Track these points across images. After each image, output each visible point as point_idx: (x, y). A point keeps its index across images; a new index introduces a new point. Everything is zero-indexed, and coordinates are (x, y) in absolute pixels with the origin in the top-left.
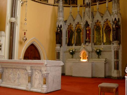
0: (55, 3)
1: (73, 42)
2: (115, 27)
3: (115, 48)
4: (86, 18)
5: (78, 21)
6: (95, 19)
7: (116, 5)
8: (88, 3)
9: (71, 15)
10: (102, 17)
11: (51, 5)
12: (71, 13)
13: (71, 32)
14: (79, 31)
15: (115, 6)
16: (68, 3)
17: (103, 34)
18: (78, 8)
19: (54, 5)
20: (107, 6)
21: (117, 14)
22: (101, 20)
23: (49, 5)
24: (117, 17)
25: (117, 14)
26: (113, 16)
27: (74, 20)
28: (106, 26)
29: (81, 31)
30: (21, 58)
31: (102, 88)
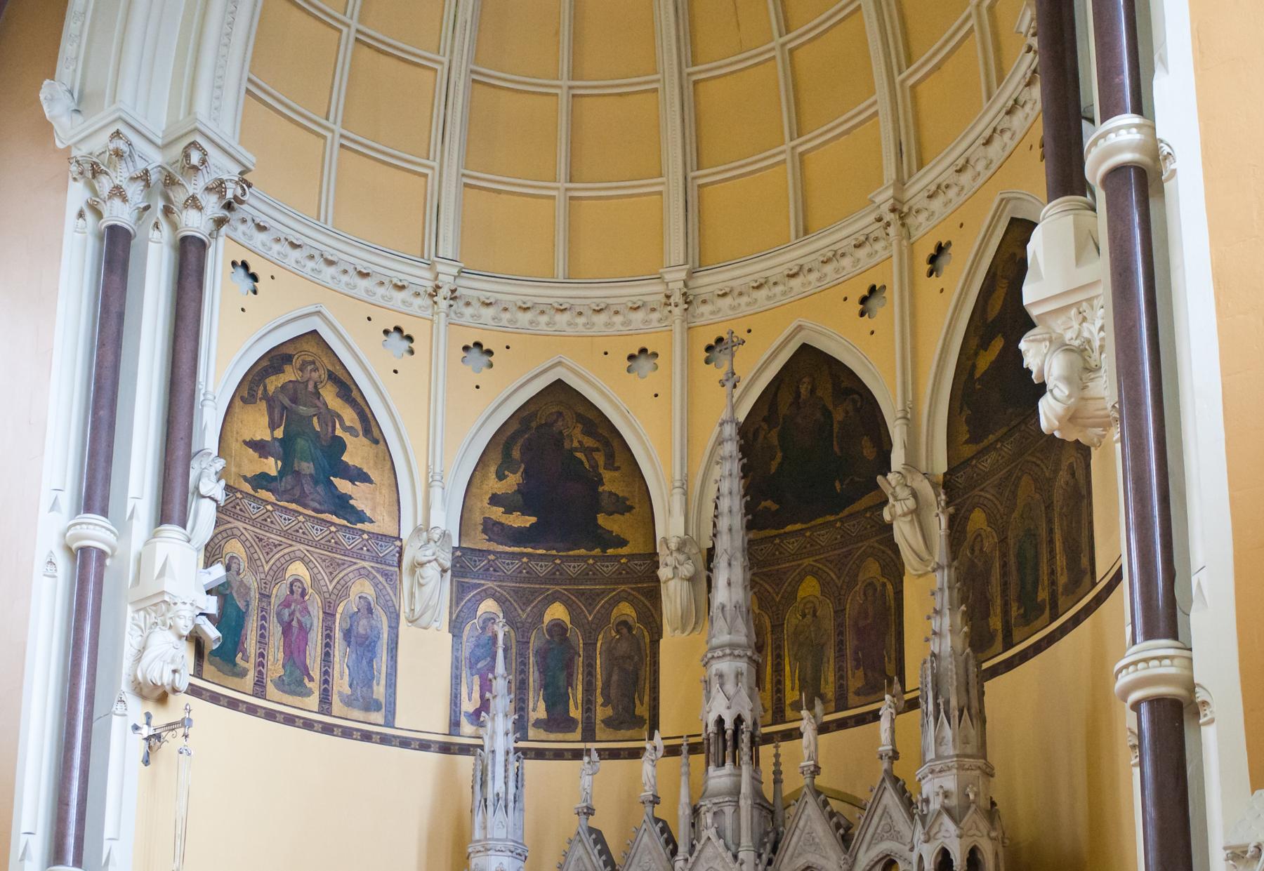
0: (455, 725)
4: (709, 851)
7: (948, 733)
8: (729, 725)
9: (585, 836)
11: (424, 746)
12: (589, 811)
15: (939, 741)
16: (573, 721)
19: (446, 749)
20: (886, 747)
23: (405, 743)
24: (960, 837)
25: (956, 812)
26: (922, 837)
30: (1024, 29)
31: (335, 422)
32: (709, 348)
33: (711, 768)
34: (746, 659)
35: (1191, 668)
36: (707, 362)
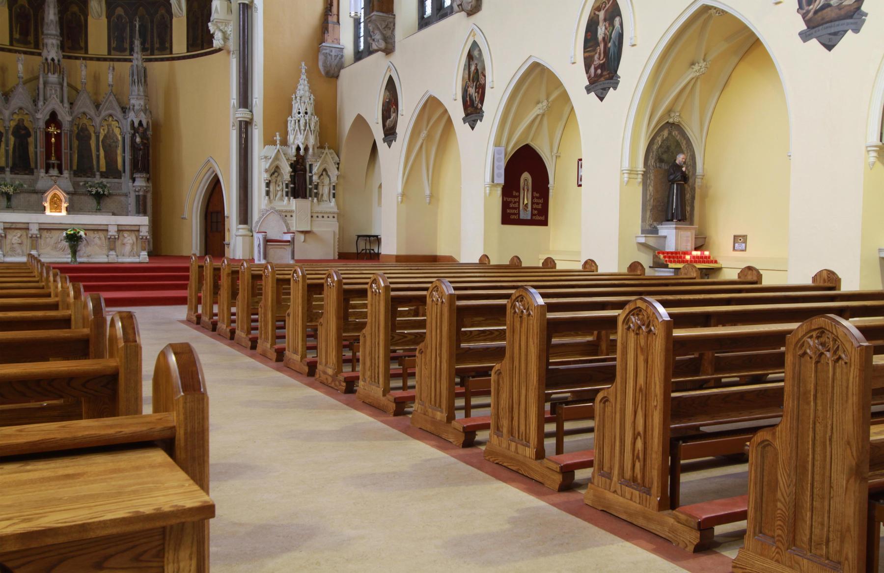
2: (142, 141)
3: (142, 189)
4: (53, 101)
5: (20, 104)
6: (76, 108)
7: (141, 89)
14: (23, 132)
15: (139, 90)
17: (98, 150)
21: (324, 173)
22: (94, 116)
23: (179, 58)
29: (28, 135)
35: (252, 115)
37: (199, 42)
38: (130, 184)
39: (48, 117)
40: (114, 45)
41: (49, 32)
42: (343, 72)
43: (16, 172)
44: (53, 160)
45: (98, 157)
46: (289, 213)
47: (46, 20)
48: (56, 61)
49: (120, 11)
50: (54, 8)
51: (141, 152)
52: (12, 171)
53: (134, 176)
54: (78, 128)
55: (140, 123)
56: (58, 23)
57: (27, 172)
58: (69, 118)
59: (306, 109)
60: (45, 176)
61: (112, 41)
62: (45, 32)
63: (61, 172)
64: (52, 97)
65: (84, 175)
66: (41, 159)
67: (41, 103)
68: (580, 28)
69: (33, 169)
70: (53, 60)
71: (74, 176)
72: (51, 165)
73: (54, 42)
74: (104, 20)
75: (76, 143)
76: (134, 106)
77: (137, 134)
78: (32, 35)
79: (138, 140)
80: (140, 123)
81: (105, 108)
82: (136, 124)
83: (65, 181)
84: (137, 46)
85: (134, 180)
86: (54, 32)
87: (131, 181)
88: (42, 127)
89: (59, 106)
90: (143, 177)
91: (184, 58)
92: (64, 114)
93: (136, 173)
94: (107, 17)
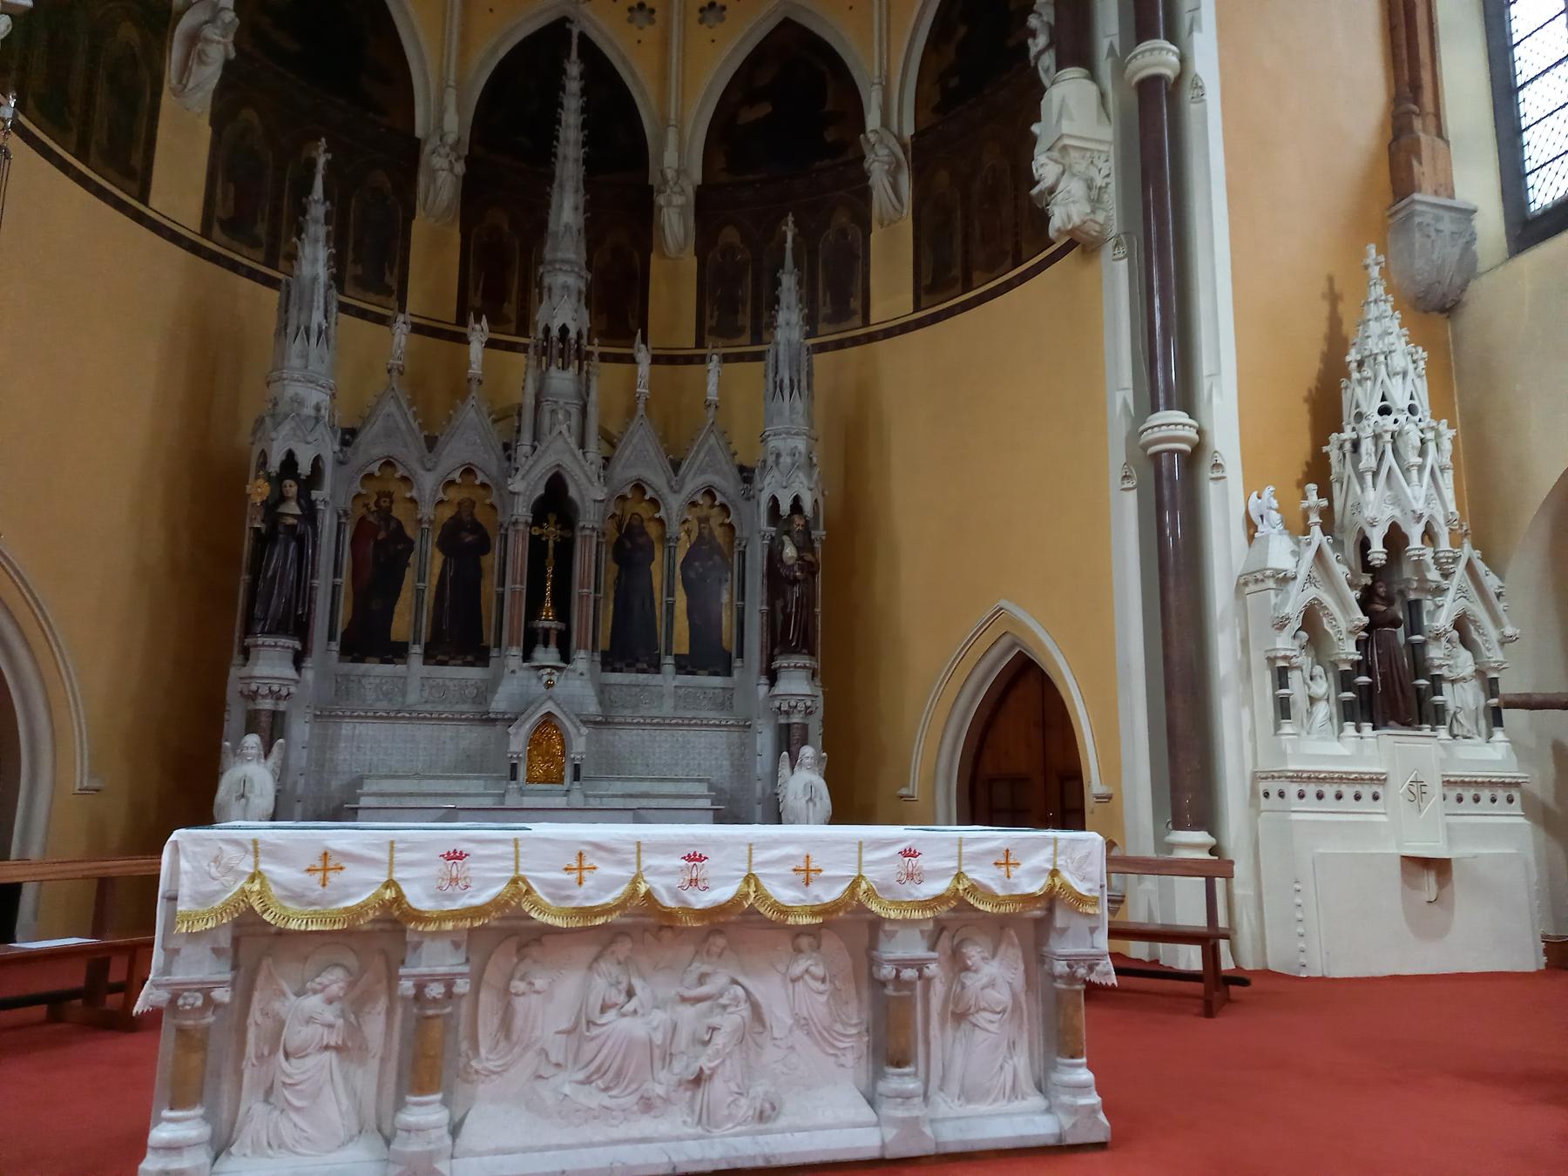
1: (400, 627)
2: (800, 558)
4: (559, 444)
6: (618, 469)
10: (676, 466)
13: (381, 536)
15: (792, 409)
17: (671, 593)
18: (400, 334)
19: (194, 248)
22: (665, 490)
23: (888, 333)
27: (431, 443)
28: (694, 536)
29: (484, 545)
32: (702, 10)
33: (553, 368)
34: (584, 280)
36: (701, 21)
37: (957, 272)
38: (763, 690)
39: (541, 491)
40: (710, 323)
41: (560, 255)
42: (1473, 285)
43: (440, 657)
44: (547, 621)
45: (670, 608)
46: (1366, 787)
47: (552, 226)
48: (573, 335)
49: (730, 235)
50: (577, 191)
51: (796, 589)
52: (429, 657)
53: (776, 664)
54: (619, 527)
55: (796, 505)
56: (583, 232)
57: (469, 658)
58: (600, 493)
59: (1412, 398)
60: (521, 668)
61: (708, 313)
62: (548, 255)
63: (566, 657)
64: (555, 433)
65: (628, 665)
66: (515, 612)
67: (525, 448)
68: (388, 805)
69: (487, 650)
70: (564, 330)
71: (603, 670)
72: (541, 637)
73: (571, 280)
74: (691, 262)
75: (610, 571)
76: (778, 456)
77: (786, 538)
78: (514, 298)
79: (790, 552)
80: (796, 505)
81: (695, 466)
82: (785, 507)
83: (578, 683)
84: (789, 289)
85: (772, 677)
86: (572, 256)
87: (764, 680)
88: (522, 519)
89: (574, 456)
90: (805, 667)
91: (905, 328)
92: (583, 480)
93: (781, 653)
94: (696, 254)
